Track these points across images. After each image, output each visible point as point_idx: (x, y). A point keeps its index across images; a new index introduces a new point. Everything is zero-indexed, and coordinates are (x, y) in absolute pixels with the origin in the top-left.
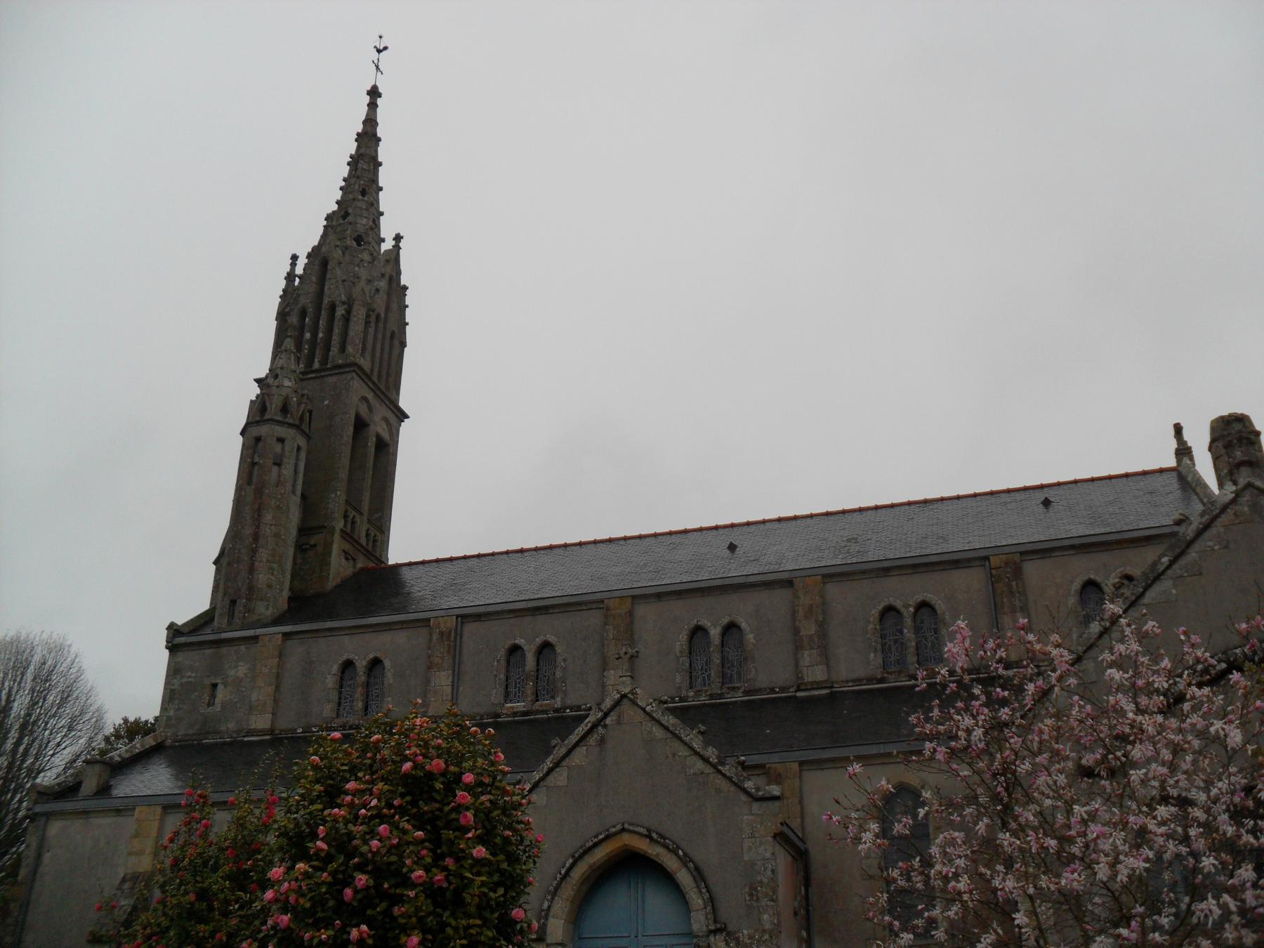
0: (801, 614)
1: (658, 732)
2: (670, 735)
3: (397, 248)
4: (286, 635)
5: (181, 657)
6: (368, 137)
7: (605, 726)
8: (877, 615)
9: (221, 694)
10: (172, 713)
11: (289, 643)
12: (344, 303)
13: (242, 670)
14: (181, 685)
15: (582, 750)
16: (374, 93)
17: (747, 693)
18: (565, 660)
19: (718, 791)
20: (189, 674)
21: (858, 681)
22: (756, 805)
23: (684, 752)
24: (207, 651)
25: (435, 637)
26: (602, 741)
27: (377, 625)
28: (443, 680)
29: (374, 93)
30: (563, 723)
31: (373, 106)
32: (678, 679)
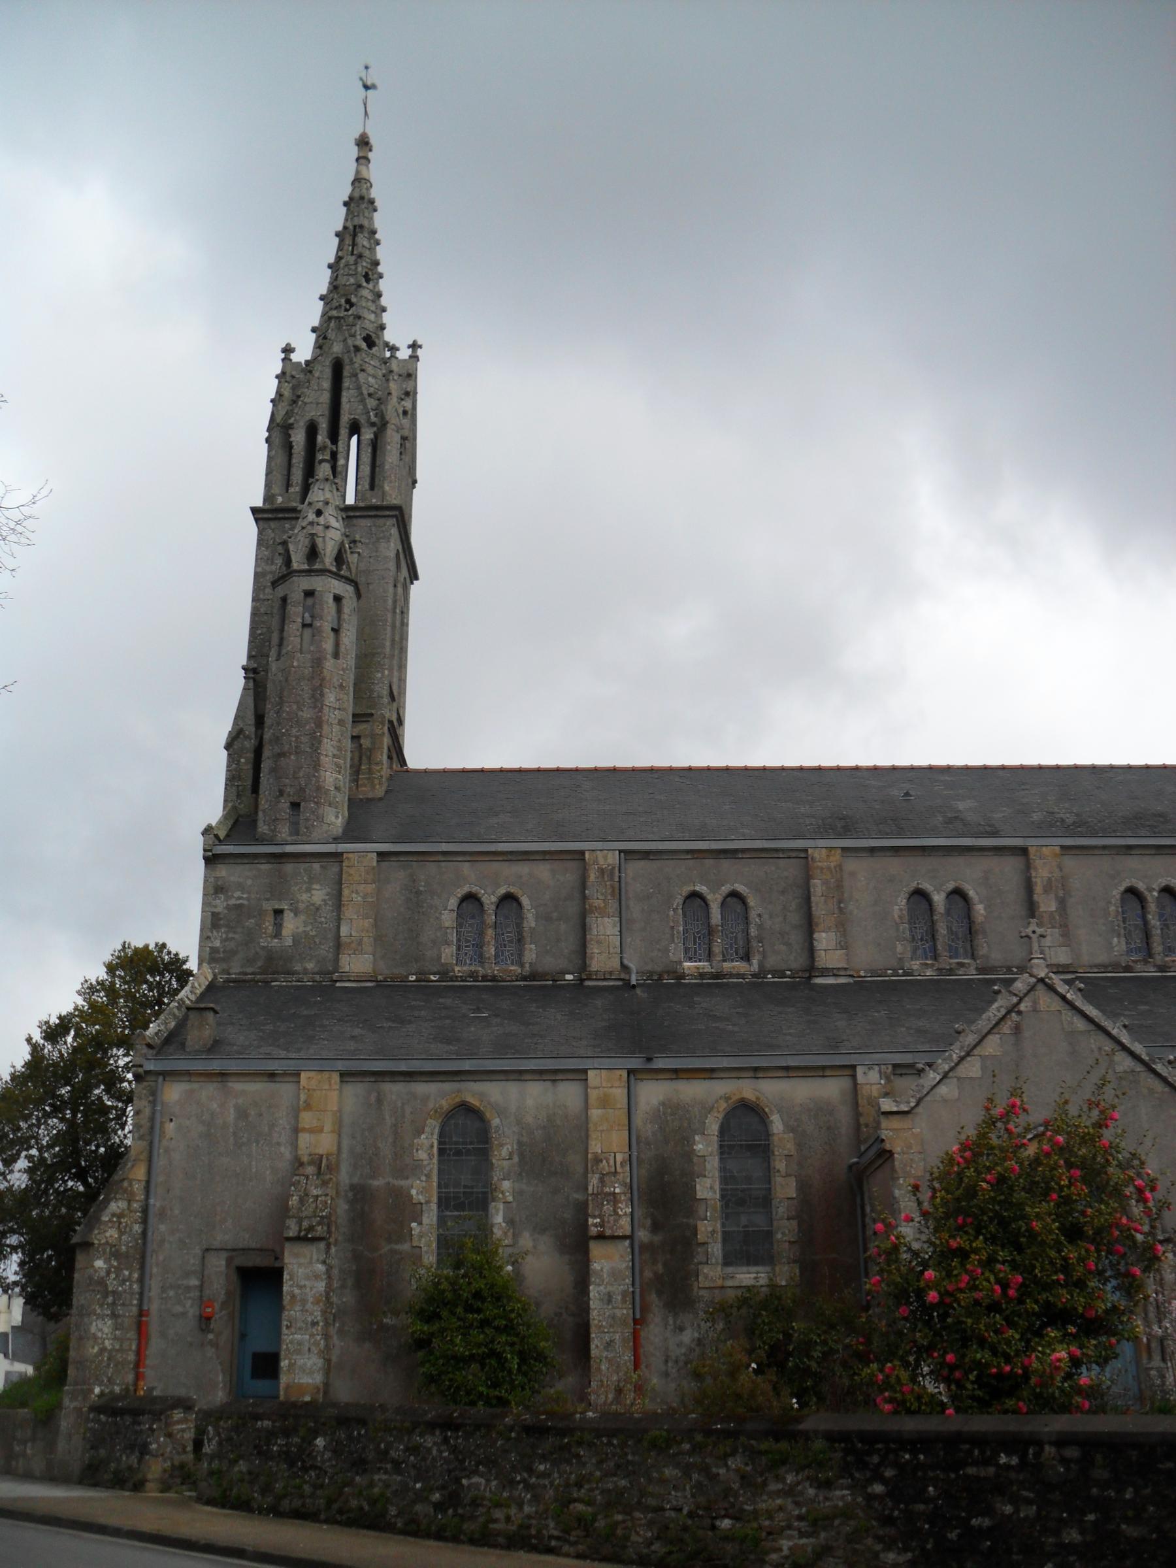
0: (1038, 889)
1: (1080, 1024)
2: (1092, 1027)
3: (414, 358)
4: (382, 855)
5: (222, 871)
6: (359, 203)
7: (1019, 1013)
8: (1118, 897)
9: (291, 924)
10: (217, 944)
11: (384, 864)
12: (373, 424)
14: (228, 908)
15: (994, 1039)
16: (363, 143)
17: (981, 970)
18: (760, 916)
19: (1151, 1091)
20: (237, 894)
21: (1104, 967)
23: (1108, 1046)
24: (263, 867)
26: (1017, 1029)
27: (511, 852)
29: (363, 143)
31: (362, 160)
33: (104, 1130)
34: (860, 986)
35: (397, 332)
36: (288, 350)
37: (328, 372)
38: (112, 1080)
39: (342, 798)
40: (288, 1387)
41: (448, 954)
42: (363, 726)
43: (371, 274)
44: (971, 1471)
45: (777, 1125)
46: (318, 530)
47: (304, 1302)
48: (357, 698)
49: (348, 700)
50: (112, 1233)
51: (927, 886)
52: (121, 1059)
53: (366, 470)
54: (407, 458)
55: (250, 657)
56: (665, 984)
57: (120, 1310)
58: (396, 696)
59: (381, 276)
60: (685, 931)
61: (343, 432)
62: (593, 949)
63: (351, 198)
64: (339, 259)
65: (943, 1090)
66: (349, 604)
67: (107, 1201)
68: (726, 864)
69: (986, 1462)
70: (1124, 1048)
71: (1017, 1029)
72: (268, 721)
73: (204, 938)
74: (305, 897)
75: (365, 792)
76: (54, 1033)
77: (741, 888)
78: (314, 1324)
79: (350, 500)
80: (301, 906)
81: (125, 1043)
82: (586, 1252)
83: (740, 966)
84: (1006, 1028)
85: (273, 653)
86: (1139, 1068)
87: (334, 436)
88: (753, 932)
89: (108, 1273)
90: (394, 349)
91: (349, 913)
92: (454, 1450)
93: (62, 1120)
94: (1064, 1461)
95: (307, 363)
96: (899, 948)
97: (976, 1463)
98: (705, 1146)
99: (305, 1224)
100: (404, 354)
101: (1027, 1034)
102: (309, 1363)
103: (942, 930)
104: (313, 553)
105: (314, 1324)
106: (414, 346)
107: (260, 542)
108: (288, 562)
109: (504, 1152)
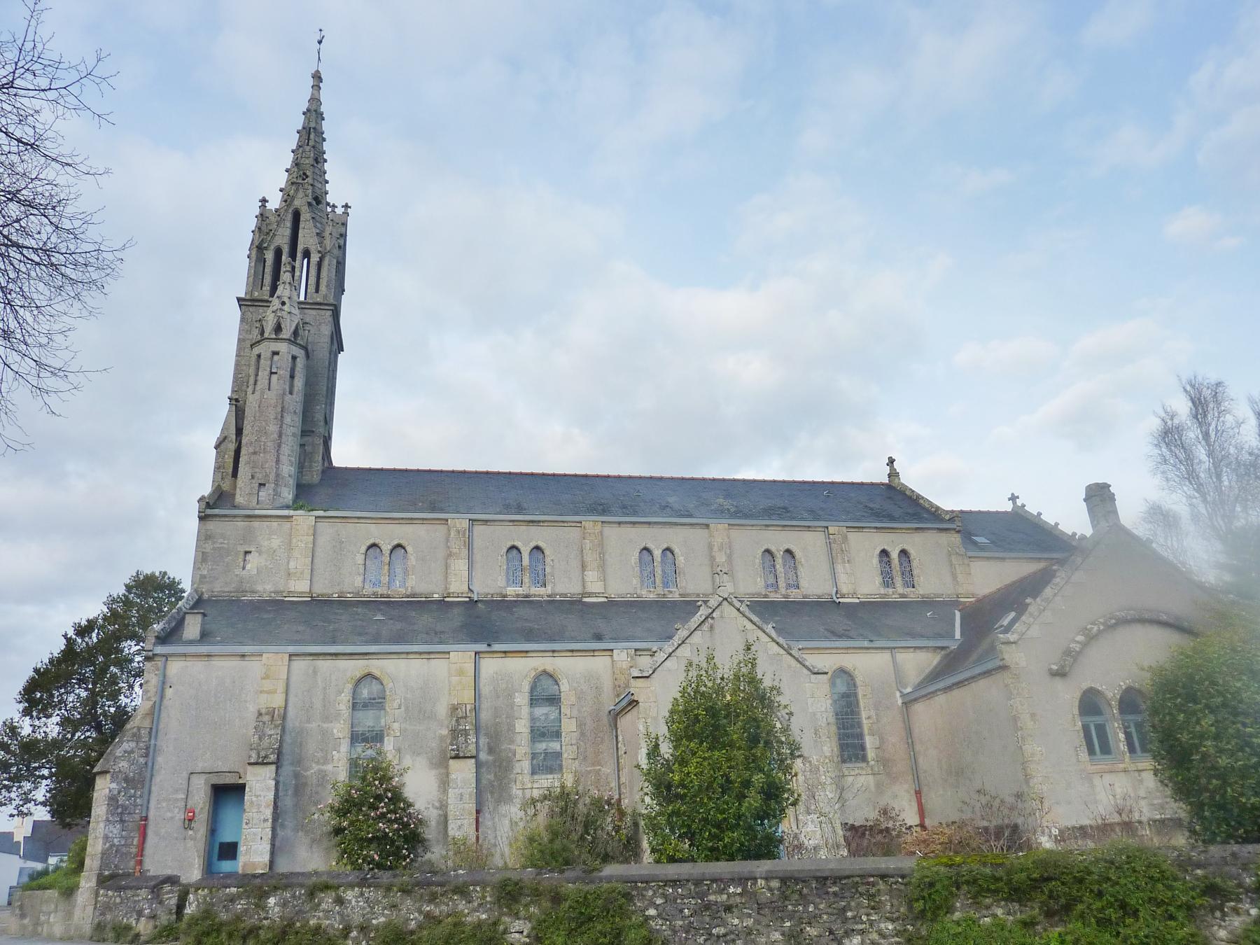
0: (716, 549)
6: (314, 114)
10: (205, 572)
13: (276, 542)
14: (214, 549)
15: (698, 633)
16: (317, 77)
19: (789, 667)
22: (813, 677)
25: (452, 534)
26: (712, 627)
28: (460, 566)
29: (317, 77)
30: (688, 607)
31: (316, 87)
32: (635, 582)
33: (114, 696)
34: (611, 604)
35: (335, 195)
36: (264, 201)
37: (289, 217)
38: (124, 662)
39: (292, 482)
40: (245, 865)
41: (358, 581)
42: (306, 439)
43: (319, 159)
44: (712, 898)
45: (565, 686)
46: (284, 314)
47: (259, 806)
48: (304, 421)
49: (298, 420)
50: (123, 765)
51: (650, 546)
52: (130, 647)
53: (312, 280)
54: (298, 287)
55: (233, 391)
56: (502, 604)
57: (126, 818)
58: (328, 421)
59: (325, 161)
60: (508, 568)
61: (299, 255)
62: (452, 578)
63: (308, 110)
64: (299, 146)
65: (667, 663)
66: (300, 363)
67: (121, 742)
68: (533, 529)
69: (721, 892)
70: (773, 640)
71: (712, 627)
72: (245, 432)
73: (196, 568)
74: (266, 543)
75: (307, 479)
76: (83, 631)
77: (541, 544)
78: (266, 820)
79: (302, 298)
80: (264, 549)
81: (134, 636)
82: (447, 767)
83: (542, 591)
84: (705, 627)
85: (250, 390)
86: (782, 652)
87: (293, 255)
88: (548, 570)
89: (119, 792)
90: (334, 206)
91: (296, 553)
92: (367, 901)
93: (86, 689)
94: (770, 889)
95: (277, 210)
96: (635, 582)
97: (714, 893)
98: (522, 699)
99: (263, 754)
100: (339, 211)
101: (717, 630)
102: (261, 848)
103: (659, 571)
104: (278, 328)
105: (266, 820)
106: (346, 206)
107: (243, 320)
108: (262, 333)
109: (395, 705)
